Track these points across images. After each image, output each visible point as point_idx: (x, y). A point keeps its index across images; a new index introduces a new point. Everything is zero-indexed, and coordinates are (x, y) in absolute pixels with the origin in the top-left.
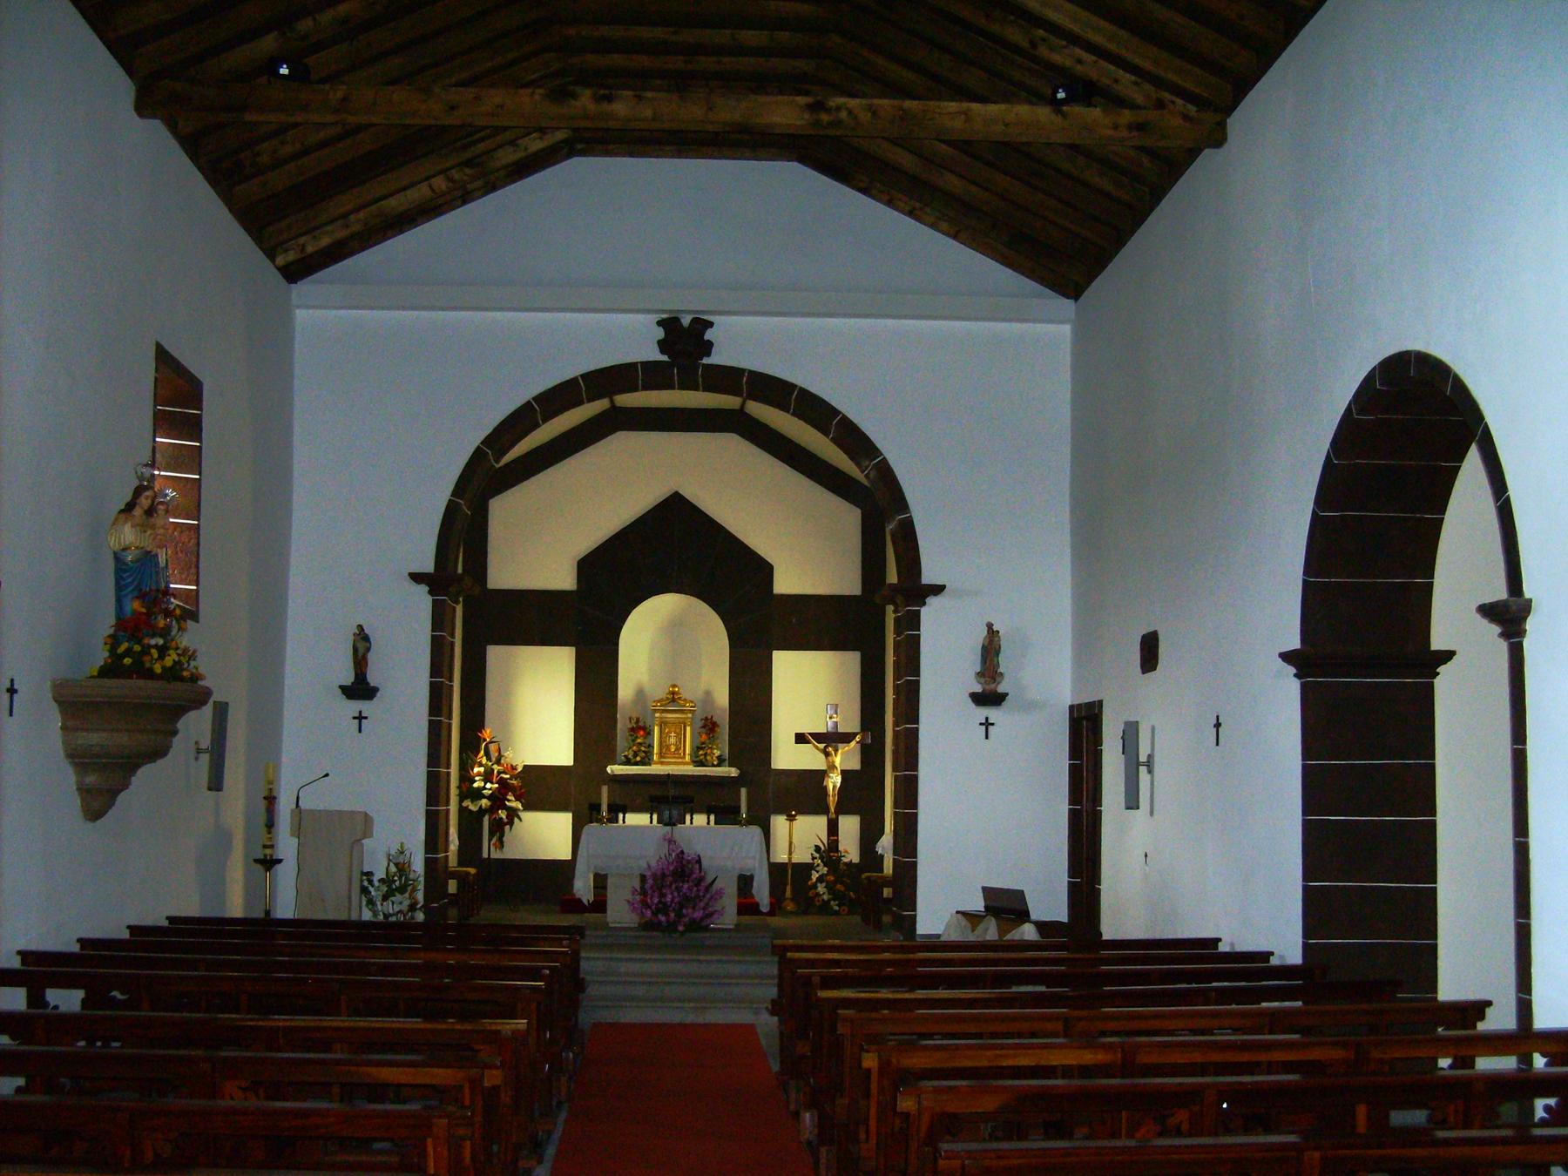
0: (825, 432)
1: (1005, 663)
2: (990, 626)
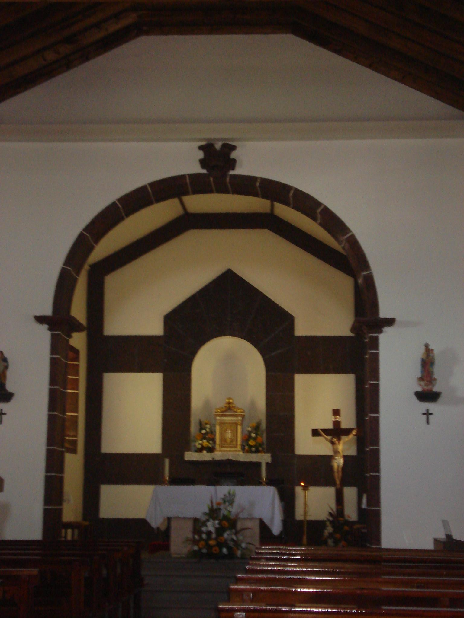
0: (314, 219)
1: (438, 371)
2: (427, 346)
